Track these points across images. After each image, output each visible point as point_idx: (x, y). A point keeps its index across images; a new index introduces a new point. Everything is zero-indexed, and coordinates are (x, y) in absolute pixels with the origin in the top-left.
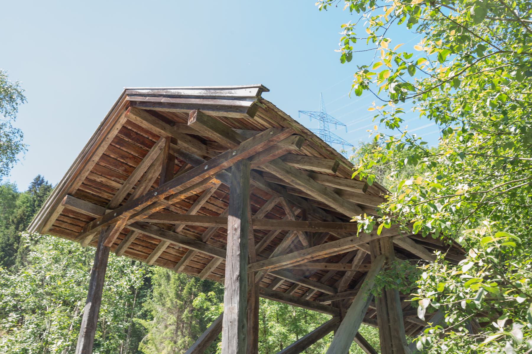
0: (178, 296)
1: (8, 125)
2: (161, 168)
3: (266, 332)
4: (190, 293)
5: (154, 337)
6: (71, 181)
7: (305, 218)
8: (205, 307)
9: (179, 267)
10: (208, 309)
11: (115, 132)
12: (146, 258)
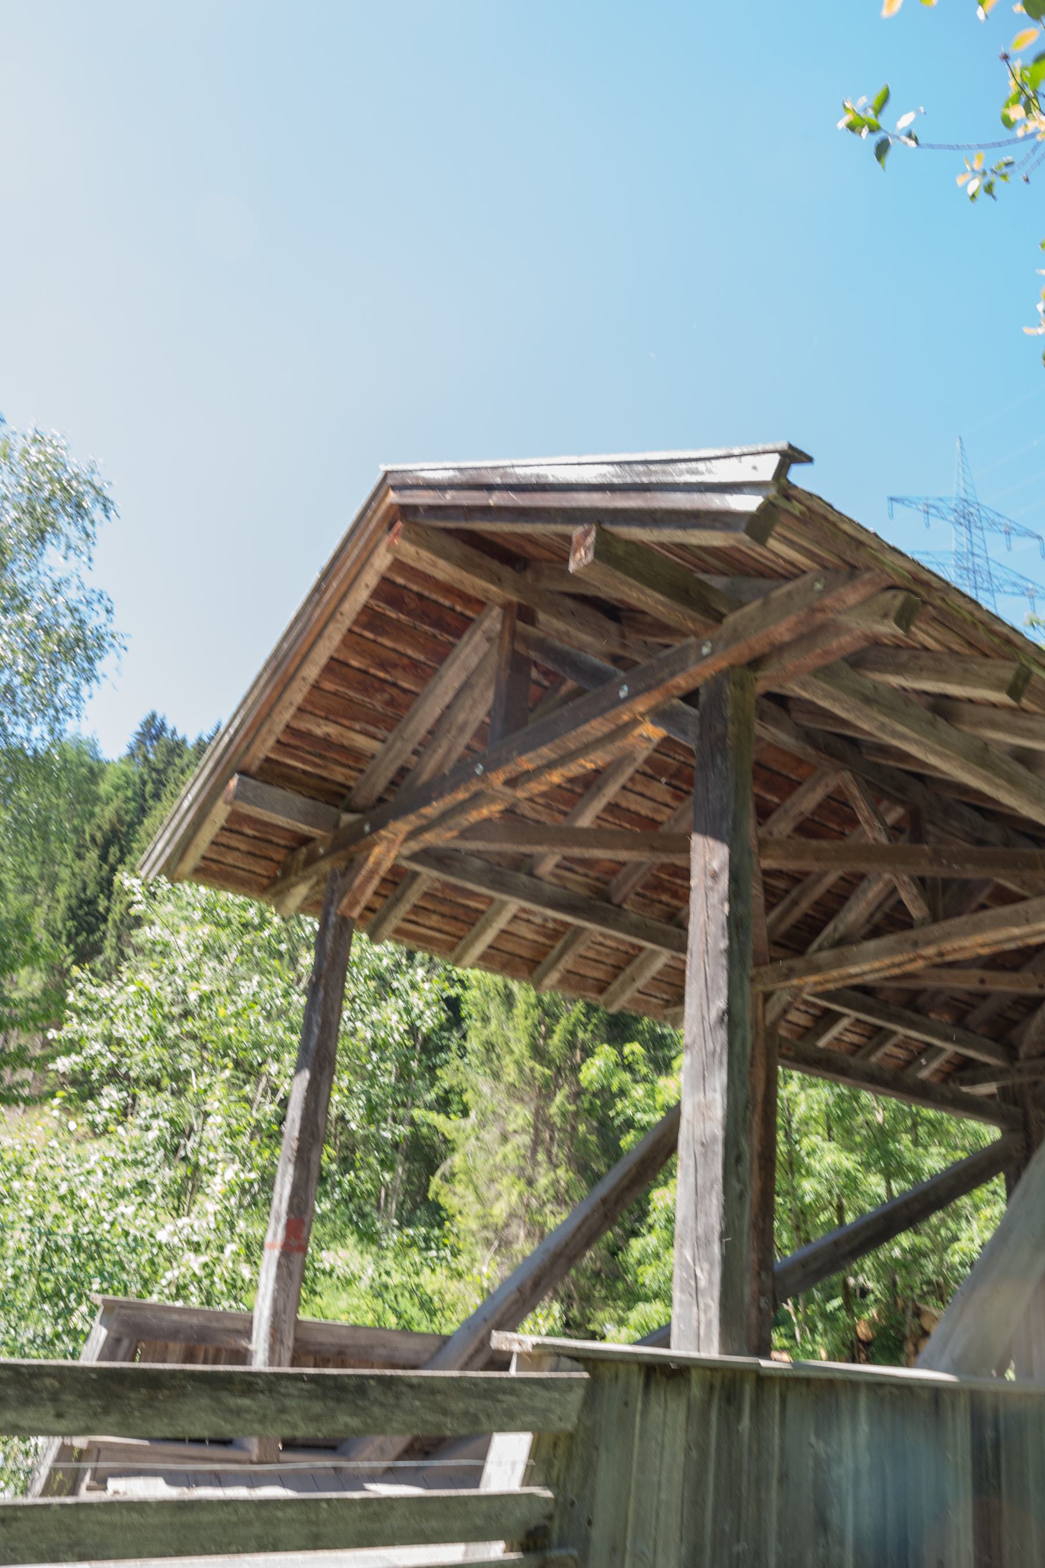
0: (538, 1053)
1: (75, 581)
2: (490, 695)
3: (794, 1165)
4: (571, 1045)
5: (471, 1163)
6: (246, 735)
7: (918, 836)
9: (545, 974)
10: (623, 1093)
11: (361, 596)
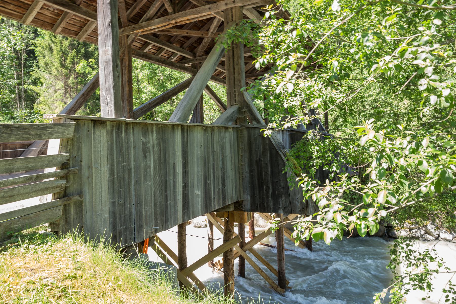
3: (139, 91)
5: (46, 99)
8: (87, 72)
9: (57, 28)
12: (21, 18)
